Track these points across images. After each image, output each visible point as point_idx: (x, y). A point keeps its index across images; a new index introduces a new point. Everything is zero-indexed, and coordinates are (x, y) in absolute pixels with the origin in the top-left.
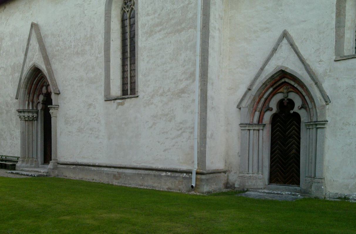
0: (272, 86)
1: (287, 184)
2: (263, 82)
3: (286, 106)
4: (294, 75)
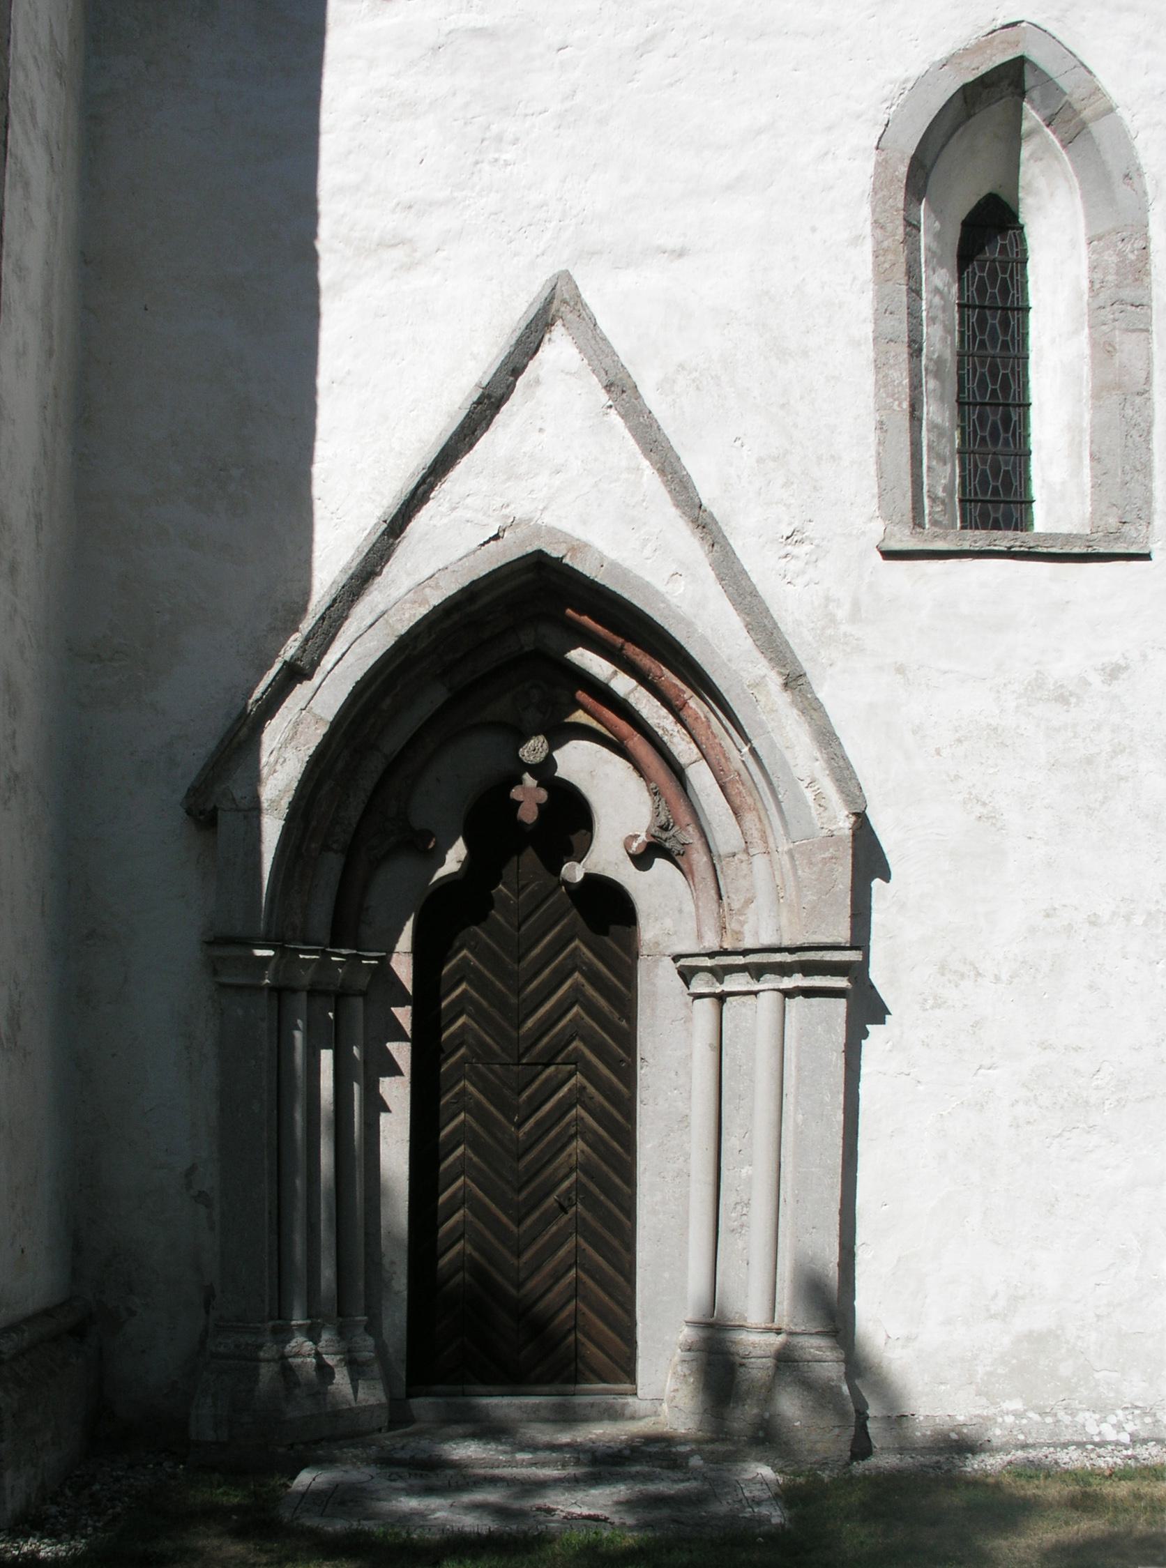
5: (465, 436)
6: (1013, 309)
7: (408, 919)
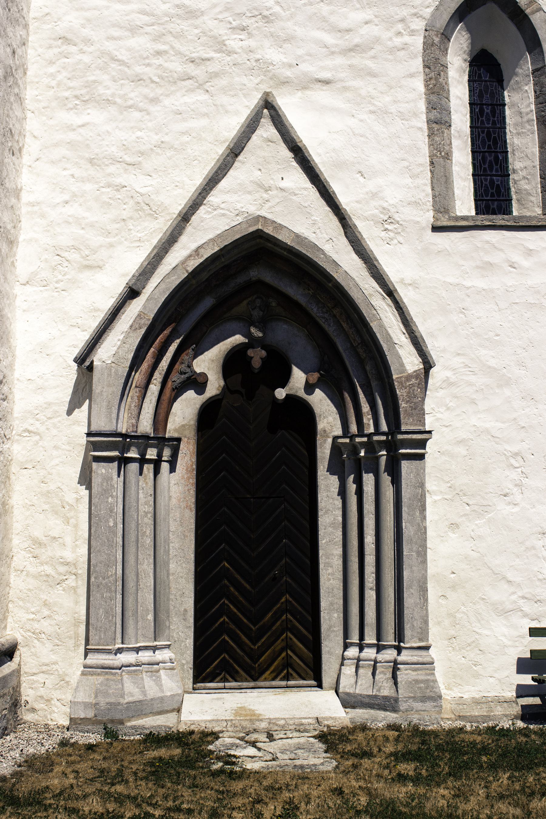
1: (265, 680)
4: (238, 236)
6: (497, 105)
7: (178, 338)
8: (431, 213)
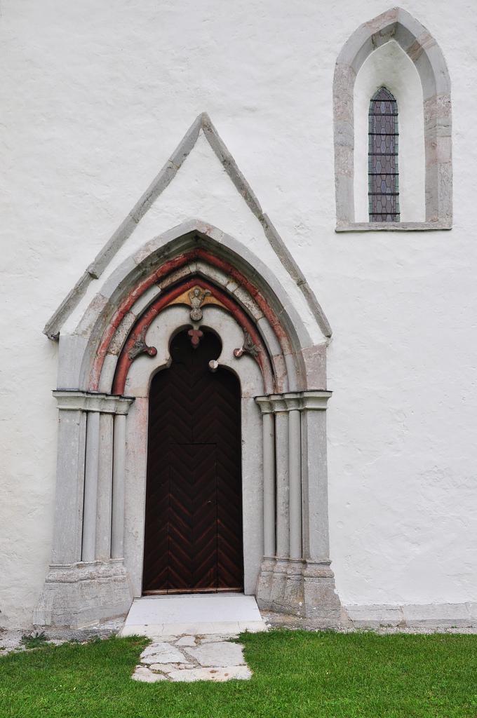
0: (158, 281)
2: (139, 261)
3: (194, 347)
5: (165, 181)
8: (335, 221)
